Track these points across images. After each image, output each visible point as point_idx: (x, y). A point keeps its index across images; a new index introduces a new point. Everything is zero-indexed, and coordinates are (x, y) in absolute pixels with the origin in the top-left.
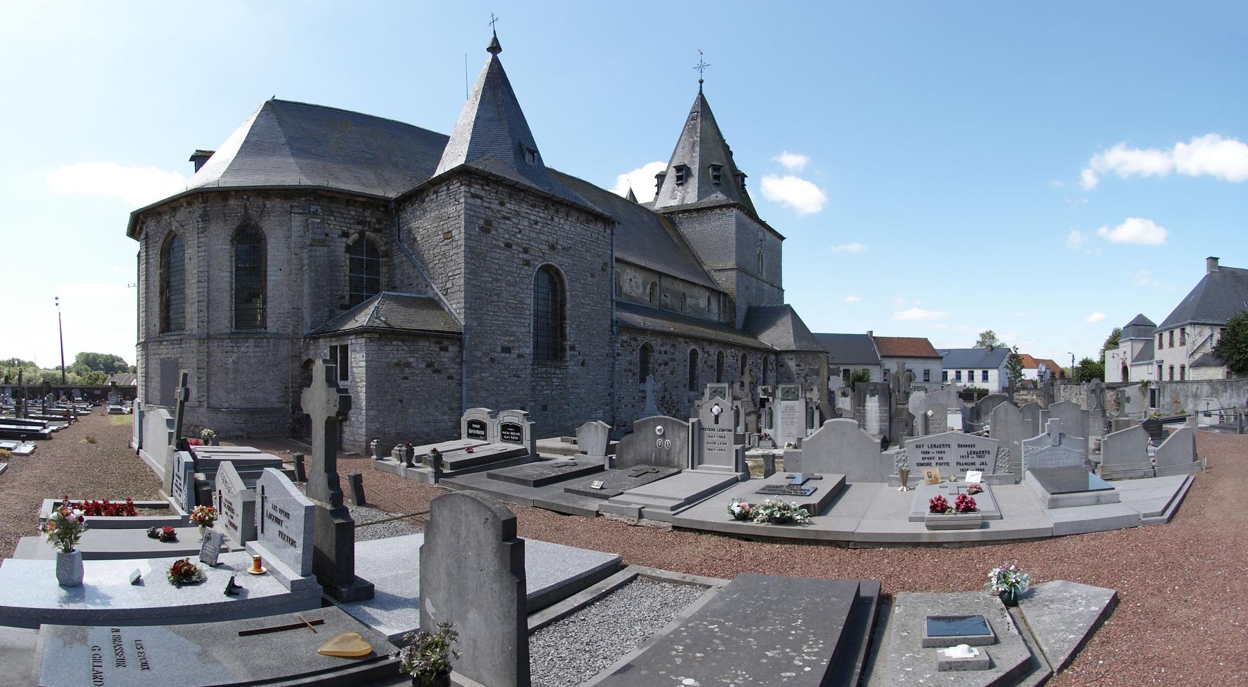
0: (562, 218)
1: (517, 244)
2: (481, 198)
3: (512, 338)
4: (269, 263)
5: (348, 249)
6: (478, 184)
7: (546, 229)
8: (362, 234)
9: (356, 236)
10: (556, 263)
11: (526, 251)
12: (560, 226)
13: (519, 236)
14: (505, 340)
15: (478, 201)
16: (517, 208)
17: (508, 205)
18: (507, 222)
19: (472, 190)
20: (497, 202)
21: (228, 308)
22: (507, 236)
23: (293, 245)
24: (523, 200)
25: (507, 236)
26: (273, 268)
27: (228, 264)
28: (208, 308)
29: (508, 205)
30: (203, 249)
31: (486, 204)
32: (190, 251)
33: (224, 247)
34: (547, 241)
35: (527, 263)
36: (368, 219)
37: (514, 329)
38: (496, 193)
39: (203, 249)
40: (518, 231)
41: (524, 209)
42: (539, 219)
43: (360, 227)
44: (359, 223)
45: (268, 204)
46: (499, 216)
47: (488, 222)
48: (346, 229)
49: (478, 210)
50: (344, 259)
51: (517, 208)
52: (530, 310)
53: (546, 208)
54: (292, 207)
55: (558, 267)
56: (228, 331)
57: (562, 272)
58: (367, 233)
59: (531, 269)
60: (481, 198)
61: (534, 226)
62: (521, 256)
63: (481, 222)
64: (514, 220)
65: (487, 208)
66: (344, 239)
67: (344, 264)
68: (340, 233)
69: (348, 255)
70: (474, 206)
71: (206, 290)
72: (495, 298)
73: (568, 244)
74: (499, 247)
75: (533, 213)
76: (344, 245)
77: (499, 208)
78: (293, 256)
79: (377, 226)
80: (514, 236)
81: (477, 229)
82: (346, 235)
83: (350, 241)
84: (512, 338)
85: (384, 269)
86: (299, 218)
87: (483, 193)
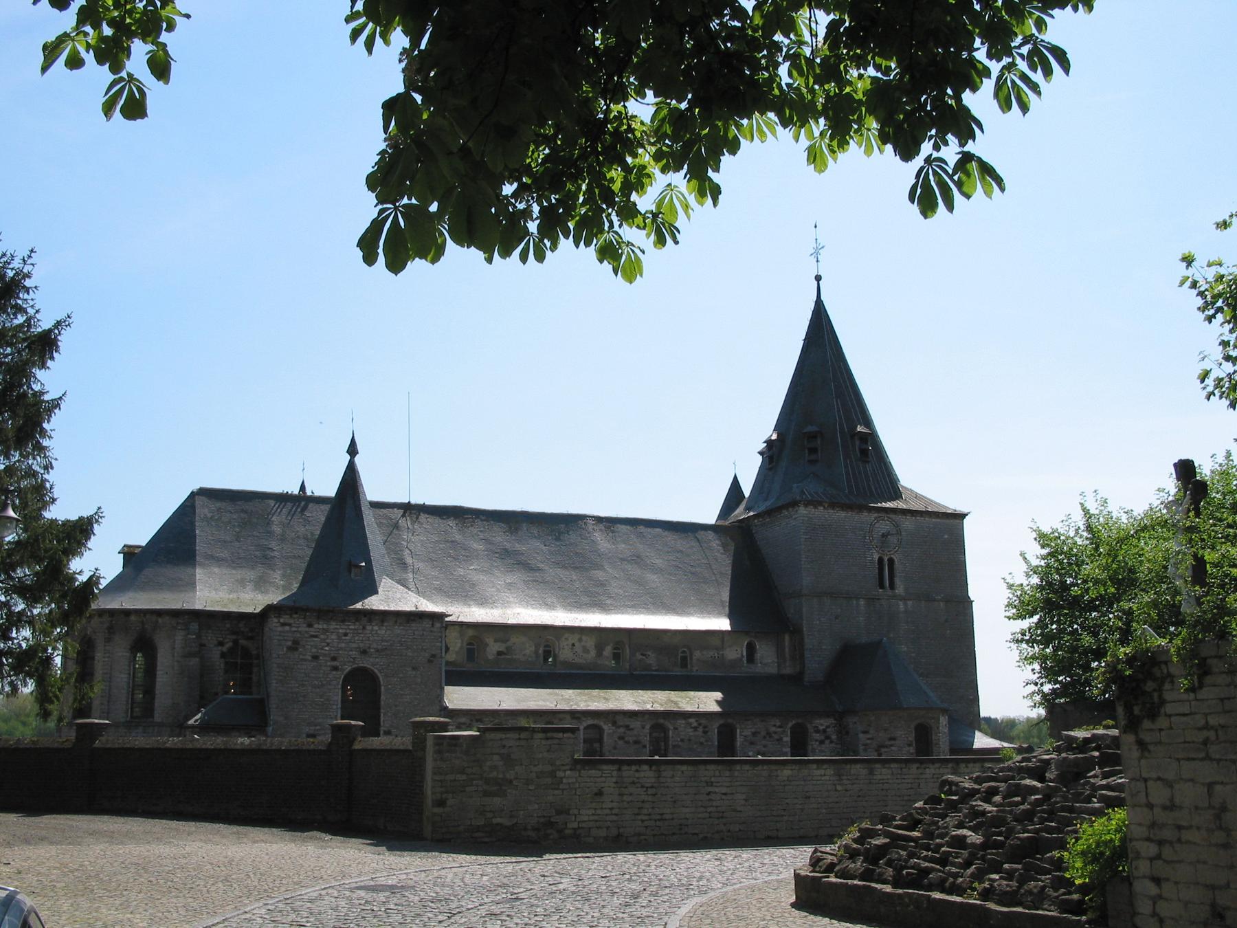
0: (376, 625)
1: (325, 655)
2: (290, 625)
3: (318, 728)
4: (158, 668)
5: (223, 655)
6: (287, 614)
7: (356, 638)
8: (235, 642)
9: (230, 644)
10: (368, 664)
11: (334, 659)
12: (374, 632)
13: (327, 648)
14: (311, 730)
15: (287, 628)
16: (325, 626)
17: (316, 626)
18: (316, 639)
19: (282, 621)
20: (305, 625)
21: (125, 703)
22: (314, 650)
23: (176, 655)
24: (331, 619)
25: (314, 650)
26: (161, 672)
27: (127, 667)
28: (109, 702)
29: (316, 626)
30: (107, 655)
31: (294, 629)
32: (99, 655)
33: (125, 654)
34: (357, 648)
35: (335, 668)
36: (242, 629)
37: (320, 720)
38: (304, 618)
39: (107, 655)
40: (326, 644)
41: (333, 625)
42: (348, 631)
43: (234, 637)
44: (234, 633)
45: (160, 620)
46: (306, 635)
47: (296, 642)
48: (221, 639)
49: (286, 634)
50: (219, 664)
51: (325, 626)
52: (337, 705)
53: (357, 620)
54: (178, 623)
55: (372, 668)
56: (122, 720)
57: (376, 671)
58: (240, 641)
59: (339, 673)
60: (290, 625)
61: (344, 638)
62: (329, 664)
63: (290, 643)
64: (322, 637)
65: (295, 631)
66: (220, 648)
67: (218, 668)
68: (216, 642)
69: (222, 660)
70: (283, 632)
71: (107, 688)
72: (301, 699)
73: (382, 646)
74: (305, 660)
75: (343, 627)
76: (219, 652)
77: (307, 629)
78: (176, 663)
79: (250, 634)
80: (322, 649)
81: (285, 649)
82: (221, 644)
83: (225, 649)
84: (318, 728)
85: (255, 670)
86: (182, 633)
87: (291, 621)
